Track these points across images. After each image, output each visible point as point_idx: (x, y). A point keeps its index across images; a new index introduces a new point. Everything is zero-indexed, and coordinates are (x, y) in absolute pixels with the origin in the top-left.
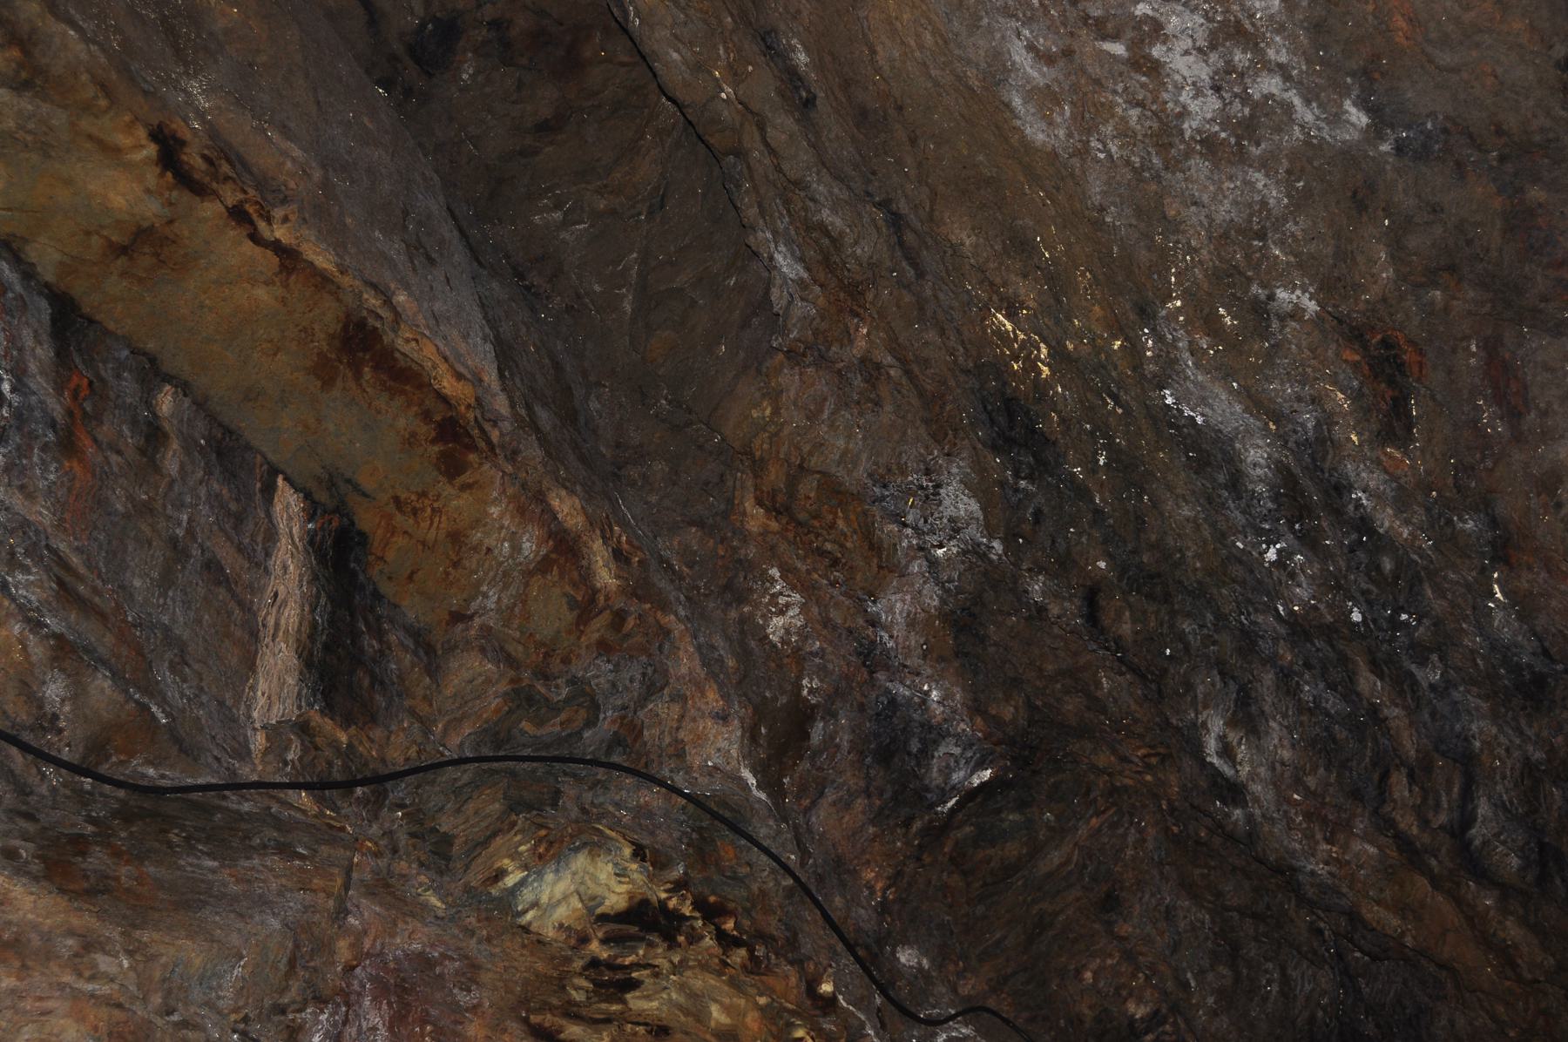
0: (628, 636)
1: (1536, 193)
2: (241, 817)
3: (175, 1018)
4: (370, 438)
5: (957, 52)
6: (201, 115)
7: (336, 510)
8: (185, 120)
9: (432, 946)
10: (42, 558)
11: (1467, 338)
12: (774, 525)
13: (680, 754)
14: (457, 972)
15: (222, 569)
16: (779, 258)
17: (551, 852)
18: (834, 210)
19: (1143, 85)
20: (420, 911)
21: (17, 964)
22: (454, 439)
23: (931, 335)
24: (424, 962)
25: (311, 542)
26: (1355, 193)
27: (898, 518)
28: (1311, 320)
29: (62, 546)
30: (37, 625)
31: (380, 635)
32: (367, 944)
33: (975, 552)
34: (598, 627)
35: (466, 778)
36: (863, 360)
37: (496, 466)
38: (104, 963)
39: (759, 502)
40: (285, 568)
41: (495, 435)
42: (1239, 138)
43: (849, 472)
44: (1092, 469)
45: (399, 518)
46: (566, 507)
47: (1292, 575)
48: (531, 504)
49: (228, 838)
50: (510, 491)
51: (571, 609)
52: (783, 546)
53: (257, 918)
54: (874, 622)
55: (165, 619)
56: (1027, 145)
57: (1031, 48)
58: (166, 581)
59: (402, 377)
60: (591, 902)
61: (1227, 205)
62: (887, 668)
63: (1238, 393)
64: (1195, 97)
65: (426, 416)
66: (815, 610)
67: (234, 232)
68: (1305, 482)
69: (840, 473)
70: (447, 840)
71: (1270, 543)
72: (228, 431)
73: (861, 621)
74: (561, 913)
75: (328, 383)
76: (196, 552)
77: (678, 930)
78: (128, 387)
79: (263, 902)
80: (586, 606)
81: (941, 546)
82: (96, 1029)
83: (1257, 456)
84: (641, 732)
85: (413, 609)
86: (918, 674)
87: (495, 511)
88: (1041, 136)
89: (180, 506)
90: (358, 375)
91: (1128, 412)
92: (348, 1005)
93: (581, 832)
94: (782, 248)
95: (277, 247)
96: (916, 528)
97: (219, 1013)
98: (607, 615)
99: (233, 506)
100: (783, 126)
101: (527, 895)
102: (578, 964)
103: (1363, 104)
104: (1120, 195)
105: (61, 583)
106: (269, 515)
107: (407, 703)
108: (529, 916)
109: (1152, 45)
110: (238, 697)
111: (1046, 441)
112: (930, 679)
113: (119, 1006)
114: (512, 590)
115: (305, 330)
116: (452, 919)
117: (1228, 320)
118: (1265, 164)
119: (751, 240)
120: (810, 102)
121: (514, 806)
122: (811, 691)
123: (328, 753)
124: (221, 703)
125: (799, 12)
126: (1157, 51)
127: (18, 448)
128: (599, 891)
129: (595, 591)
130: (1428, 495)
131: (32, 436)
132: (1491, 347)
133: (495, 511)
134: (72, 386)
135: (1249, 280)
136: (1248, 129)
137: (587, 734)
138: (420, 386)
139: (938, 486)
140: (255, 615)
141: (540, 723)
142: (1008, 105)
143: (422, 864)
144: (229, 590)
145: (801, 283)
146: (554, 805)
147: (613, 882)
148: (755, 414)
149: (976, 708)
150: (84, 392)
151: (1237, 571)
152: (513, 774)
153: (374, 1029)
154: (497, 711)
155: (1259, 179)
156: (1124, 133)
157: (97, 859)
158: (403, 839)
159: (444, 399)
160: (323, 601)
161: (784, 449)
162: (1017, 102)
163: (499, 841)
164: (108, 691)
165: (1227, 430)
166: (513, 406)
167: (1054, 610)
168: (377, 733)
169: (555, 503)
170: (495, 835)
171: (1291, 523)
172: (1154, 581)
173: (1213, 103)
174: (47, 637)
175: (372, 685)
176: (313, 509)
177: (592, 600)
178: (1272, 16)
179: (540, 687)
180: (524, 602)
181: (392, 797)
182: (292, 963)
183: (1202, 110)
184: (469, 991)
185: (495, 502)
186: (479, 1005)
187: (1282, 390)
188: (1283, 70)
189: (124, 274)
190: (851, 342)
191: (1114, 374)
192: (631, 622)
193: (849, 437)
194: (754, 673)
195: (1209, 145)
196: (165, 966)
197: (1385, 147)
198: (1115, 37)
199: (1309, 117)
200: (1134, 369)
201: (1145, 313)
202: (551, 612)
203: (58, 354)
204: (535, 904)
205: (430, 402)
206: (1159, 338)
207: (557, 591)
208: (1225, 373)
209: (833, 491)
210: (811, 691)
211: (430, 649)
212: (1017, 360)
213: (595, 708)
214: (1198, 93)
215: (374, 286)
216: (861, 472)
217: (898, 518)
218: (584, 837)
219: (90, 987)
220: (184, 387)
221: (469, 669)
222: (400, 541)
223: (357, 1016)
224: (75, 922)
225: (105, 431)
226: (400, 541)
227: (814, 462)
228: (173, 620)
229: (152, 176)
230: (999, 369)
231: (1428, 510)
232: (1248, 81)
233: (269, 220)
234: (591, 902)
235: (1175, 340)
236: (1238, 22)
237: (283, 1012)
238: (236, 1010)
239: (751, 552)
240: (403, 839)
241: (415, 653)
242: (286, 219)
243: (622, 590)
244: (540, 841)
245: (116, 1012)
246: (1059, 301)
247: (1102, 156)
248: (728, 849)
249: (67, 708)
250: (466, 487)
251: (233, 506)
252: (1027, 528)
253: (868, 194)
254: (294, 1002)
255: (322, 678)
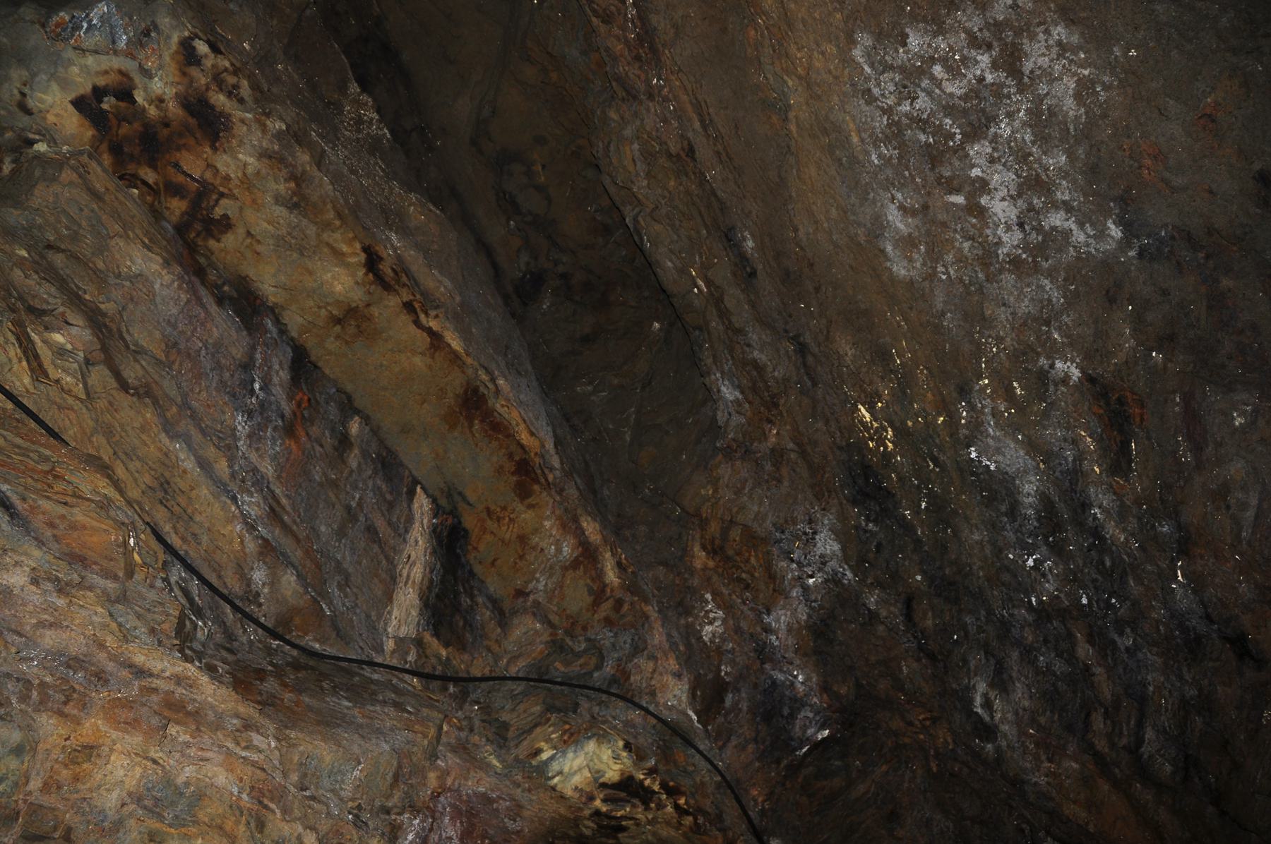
0: (623, 616)
1: (1226, 282)
2: (372, 681)
3: (307, 793)
4: (476, 468)
5: (852, 218)
6: (395, 249)
7: (451, 513)
8: (386, 248)
9: (492, 790)
10: (262, 490)
11: (1174, 392)
12: (711, 564)
13: (653, 694)
14: (507, 808)
15: (377, 533)
16: (723, 389)
17: (571, 739)
18: (761, 351)
19: (973, 226)
20: (485, 767)
21: (194, 727)
22: (525, 474)
23: (820, 425)
24: (486, 799)
25: (434, 531)
26: (1108, 292)
27: (787, 555)
28: (1075, 386)
29: (277, 491)
30: (251, 528)
31: (472, 597)
32: (449, 782)
33: (834, 579)
34: (606, 608)
35: (520, 689)
36: (773, 450)
37: (551, 496)
38: (257, 739)
39: (704, 548)
40: (417, 542)
41: (550, 477)
42: (1034, 257)
43: (760, 525)
44: (917, 511)
45: (489, 522)
46: (591, 528)
47: (1044, 575)
48: (570, 524)
49: (362, 693)
50: (557, 512)
51: (590, 595)
52: (715, 578)
53: (374, 741)
54: (768, 630)
55: (339, 557)
56: (893, 279)
57: (902, 208)
58: (341, 533)
59: (497, 428)
60: (597, 774)
61: (1026, 302)
62: (771, 660)
63: (1022, 441)
64: (1006, 232)
65: (510, 456)
66: (731, 622)
67: (405, 319)
68: (1061, 506)
69: (755, 525)
70: (505, 726)
71: (1030, 555)
72: (389, 450)
73: (759, 629)
74: (577, 780)
75: (452, 427)
76: (362, 519)
77: (651, 800)
78: (333, 411)
79: (379, 732)
80: (599, 594)
81: (812, 577)
82: (241, 780)
83: (1029, 488)
84: (629, 678)
85: (494, 585)
86: (791, 663)
87: (547, 524)
88: (903, 272)
89: (356, 488)
90: (471, 426)
91: (943, 469)
92: (433, 817)
93: (591, 727)
94: (726, 382)
95: (430, 331)
96: (799, 563)
97: (341, 800)
98: (611, 601)
99: (388, 497)
100: (734, 297)
101: (555, 766)
102: (587, 812)
103: (1120, 222)
104: (955, 305)
105: (271, 507)
106: (410, 510)
107: (485, 643)
108: (556, 780)
109: (981, 196)
110: (380, 616)
111: (889, 494)
112: (798, 667)
113: (263, 770)
114: (554, 579)
115: (441, 389)
116: (506, 776)
117: (1018, 391)
118: (1051, 274)
119: (707, 381)
120: (753, 274)
121: (550, 709)
122: (726, 673)
123: (433, 660)
124: (368, 616)
125: (750, 212)
126: (984, 201)
127: (259, 424)
128: (603, 767)
129: (605, 585)
130: (1141, 508)
131: (268, 420)
132: (1188, 399)
133: (547, 524)
134: (298, 398)
135: (1038, 354)
136: (1039, 250)
137: (596, 675)
138: (508, 436)
139: (815, 533)
140: (395, 567)
141: (567, 663)
142: (883, 251)
143: (488, 740)
144: (381, 547)
145: (737, 401)
146: (575, 712)
147: (611, 762)
148: (703, 492)
149: (825, 688)
150: (304, 405)
151: (1006, 577)
152: (549, 690)
153: (450, 838)
154: (542, 652)
155: (1046, 283)
156: (961, 259)
157: (271, 685)
158: (477, 723)
159: (522, 447)
160: (438, 566)
161: (720, 512)
162: (889, 248)
163: (538, 730)
164: (293, 584)
165: (1011, 470)
166: (562, 463)
167: (884, 613)
168: (466, 657)
169: (585, 525)
170: (536, 726)
171: (1046, 538)
172: (950, 588)
173: (1018, 235)
174: (257, 537)
175: (464, 626)
176: (437, 510)
177: (603, 591)
178: (1060, 168)
179: (568, 641)
180: (561, 587)
181: (473, 696)
182: (396, 777)
183: (1010, 240)
184: (515, 821)
185: (548, 518)
186: (521, 831)
187: (1053, 434)
188: (1068, 207)
189: (338, 337)
190: (766, 439)
191: (937, 441)
192: (626, 607)
193: (760, 504)
194: (695, 656)
195: (1015, 262)
196: (302, 754)
197: (1132, 253)
198: (957, 191)
199: (1082, 238)
200: (951, 436)
201: (964, 391)
202: (577, 597)
203: (292, 379)
204: (560, 773)
205: (513, 448)
206: (971, 407)
207: (582, 582)
208: (1012, 427)
209: (752, 539)
210: (726, 673)
211: (502, 613)
212: (872, 440)
213: (602, 658)
214: (1008, 228)
215: (486, 369)
216: (768, 523)
217: (787, 555)
218: (594, 730)
219: (244, 754)
220: (366, 419)
221: (526, 628)
222: (489, 538)
223: (439, 827)
224: (241, 709)
225: (315, 431)
226: (489, 538)
227: (740, 518)
228: (344, 558)
229: (361, 273)
230: (861, 447)
231: (1140, 519)
232: (1041, 217)
233: (427, 314)
234: (597, 774)
235: (983, 407)
236: (1038, 175)
237: (388, 812)
238: (353, 800)
239: (696, 582)
240: (477, 723)
241: (492, 612)
242: (437, 316)
243: (622, 586)
244: (565, 732)
245: (258, 772)
246: (904, 393)
247: (944, 277)
248: (682, 754)
249: (266, 590)
250: (530, 506)
251: (388, 497)
252: (871, 555)
253: (786, 331)
254: (396, 806)
255: (433, 615)
